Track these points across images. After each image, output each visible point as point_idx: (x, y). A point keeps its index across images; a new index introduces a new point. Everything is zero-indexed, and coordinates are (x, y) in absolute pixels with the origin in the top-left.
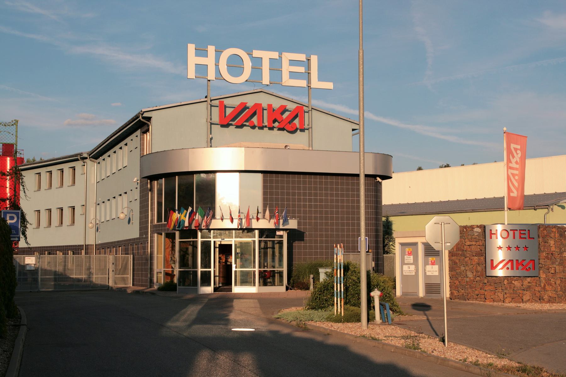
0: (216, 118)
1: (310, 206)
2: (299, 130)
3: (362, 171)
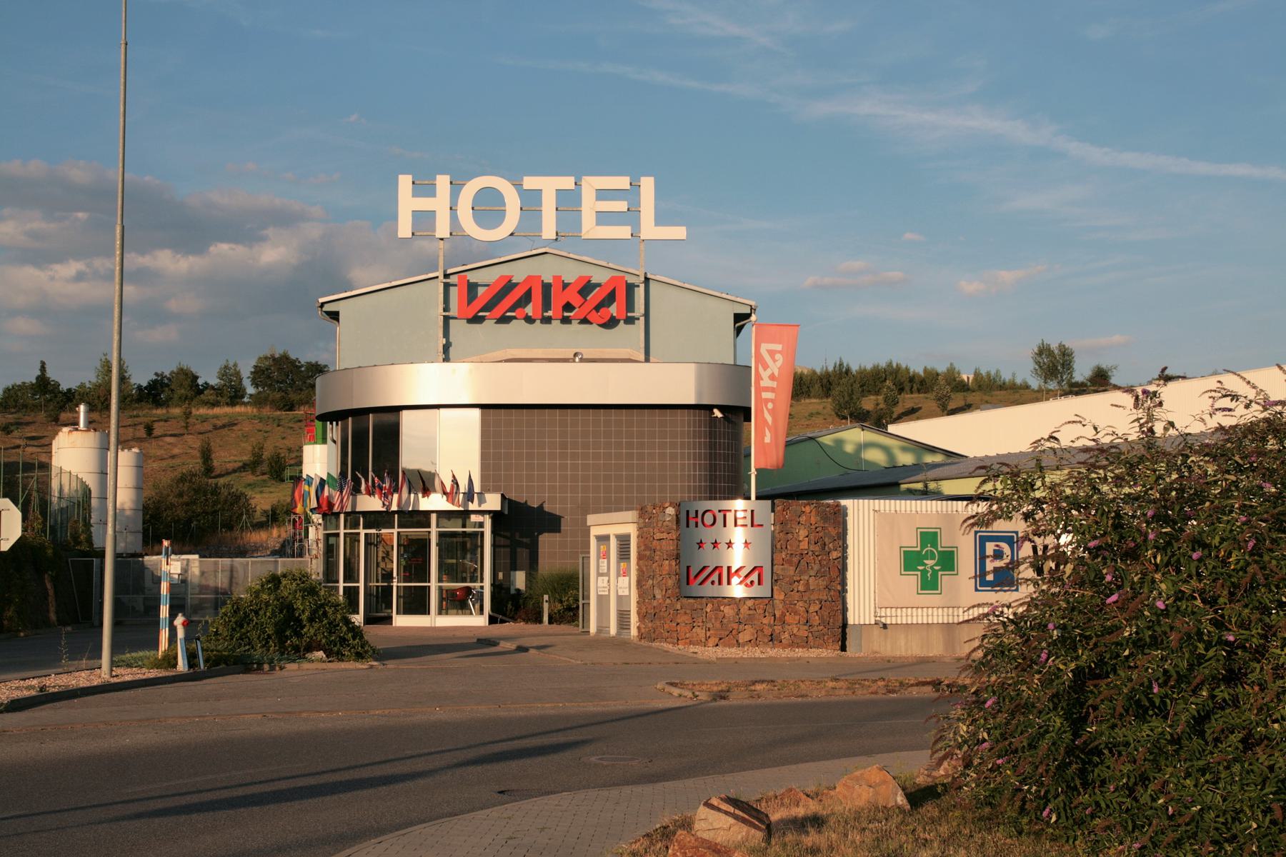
2: (622, 322)
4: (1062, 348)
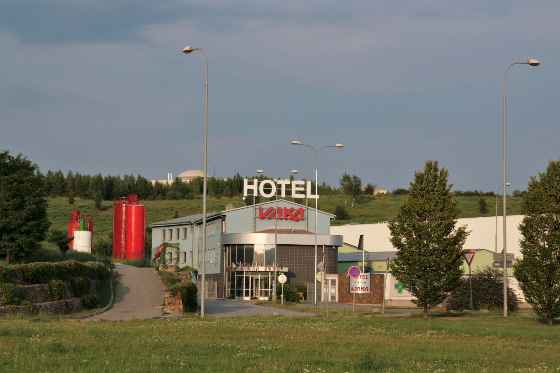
0: (258, 215)
1: (299, 260)
3: (504, 193)
4: (355, 177)
